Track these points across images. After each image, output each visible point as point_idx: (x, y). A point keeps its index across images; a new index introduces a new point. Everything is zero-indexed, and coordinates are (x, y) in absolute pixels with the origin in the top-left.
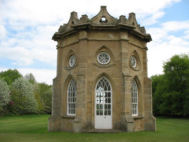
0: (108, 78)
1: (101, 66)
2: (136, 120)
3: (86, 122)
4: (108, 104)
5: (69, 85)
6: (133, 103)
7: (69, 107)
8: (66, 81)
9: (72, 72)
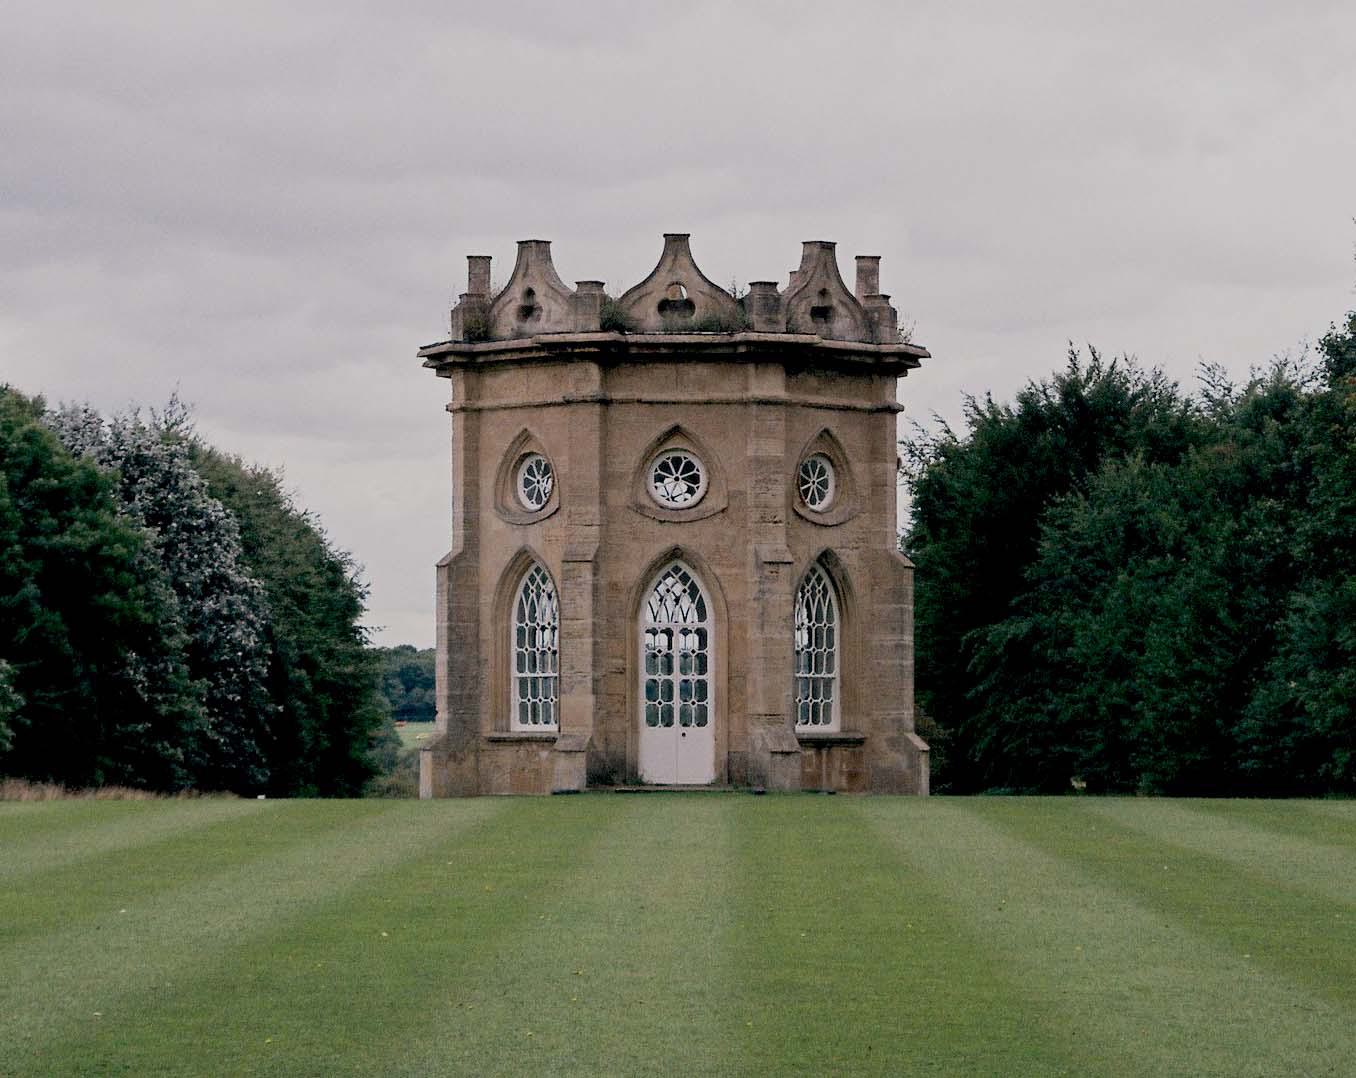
0: (694, 568)
1: (667, 517)
2: (824, 752)
3: (603, 756)
4: (693, 677)
5: (520, 593)
6: (811, 675)
7: (523, 695)
8: (504, 576)
9: (534, 539)
